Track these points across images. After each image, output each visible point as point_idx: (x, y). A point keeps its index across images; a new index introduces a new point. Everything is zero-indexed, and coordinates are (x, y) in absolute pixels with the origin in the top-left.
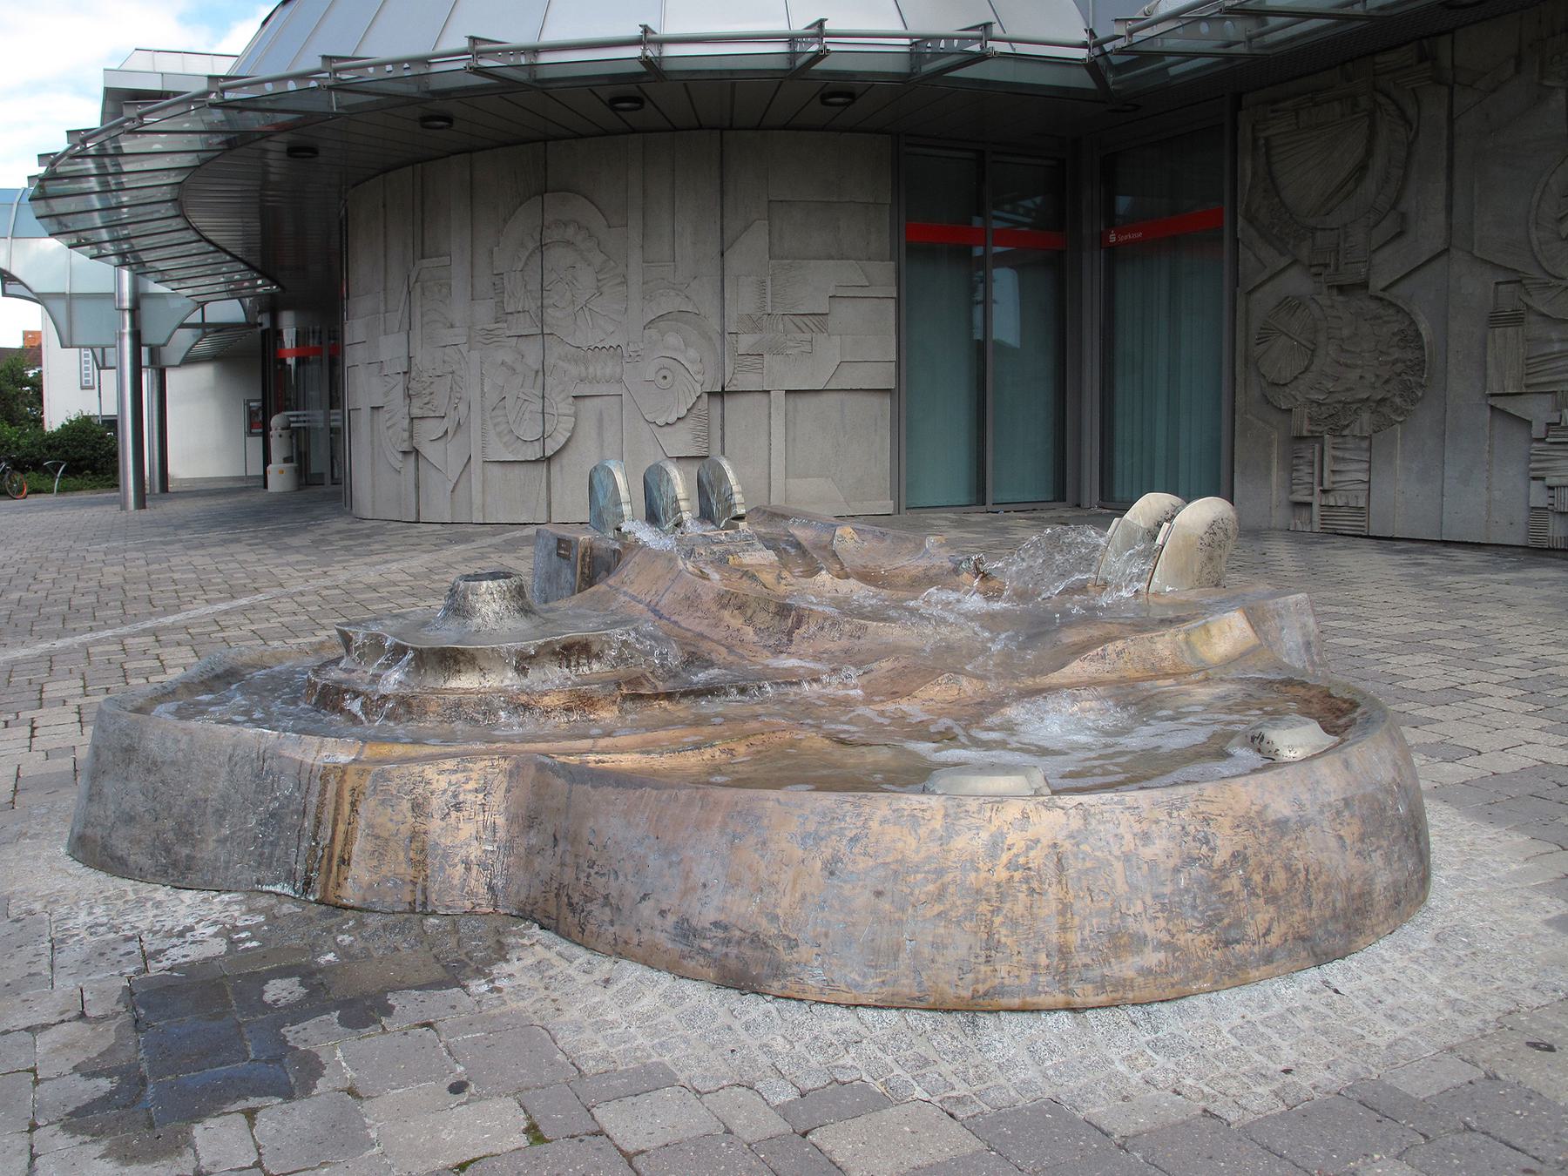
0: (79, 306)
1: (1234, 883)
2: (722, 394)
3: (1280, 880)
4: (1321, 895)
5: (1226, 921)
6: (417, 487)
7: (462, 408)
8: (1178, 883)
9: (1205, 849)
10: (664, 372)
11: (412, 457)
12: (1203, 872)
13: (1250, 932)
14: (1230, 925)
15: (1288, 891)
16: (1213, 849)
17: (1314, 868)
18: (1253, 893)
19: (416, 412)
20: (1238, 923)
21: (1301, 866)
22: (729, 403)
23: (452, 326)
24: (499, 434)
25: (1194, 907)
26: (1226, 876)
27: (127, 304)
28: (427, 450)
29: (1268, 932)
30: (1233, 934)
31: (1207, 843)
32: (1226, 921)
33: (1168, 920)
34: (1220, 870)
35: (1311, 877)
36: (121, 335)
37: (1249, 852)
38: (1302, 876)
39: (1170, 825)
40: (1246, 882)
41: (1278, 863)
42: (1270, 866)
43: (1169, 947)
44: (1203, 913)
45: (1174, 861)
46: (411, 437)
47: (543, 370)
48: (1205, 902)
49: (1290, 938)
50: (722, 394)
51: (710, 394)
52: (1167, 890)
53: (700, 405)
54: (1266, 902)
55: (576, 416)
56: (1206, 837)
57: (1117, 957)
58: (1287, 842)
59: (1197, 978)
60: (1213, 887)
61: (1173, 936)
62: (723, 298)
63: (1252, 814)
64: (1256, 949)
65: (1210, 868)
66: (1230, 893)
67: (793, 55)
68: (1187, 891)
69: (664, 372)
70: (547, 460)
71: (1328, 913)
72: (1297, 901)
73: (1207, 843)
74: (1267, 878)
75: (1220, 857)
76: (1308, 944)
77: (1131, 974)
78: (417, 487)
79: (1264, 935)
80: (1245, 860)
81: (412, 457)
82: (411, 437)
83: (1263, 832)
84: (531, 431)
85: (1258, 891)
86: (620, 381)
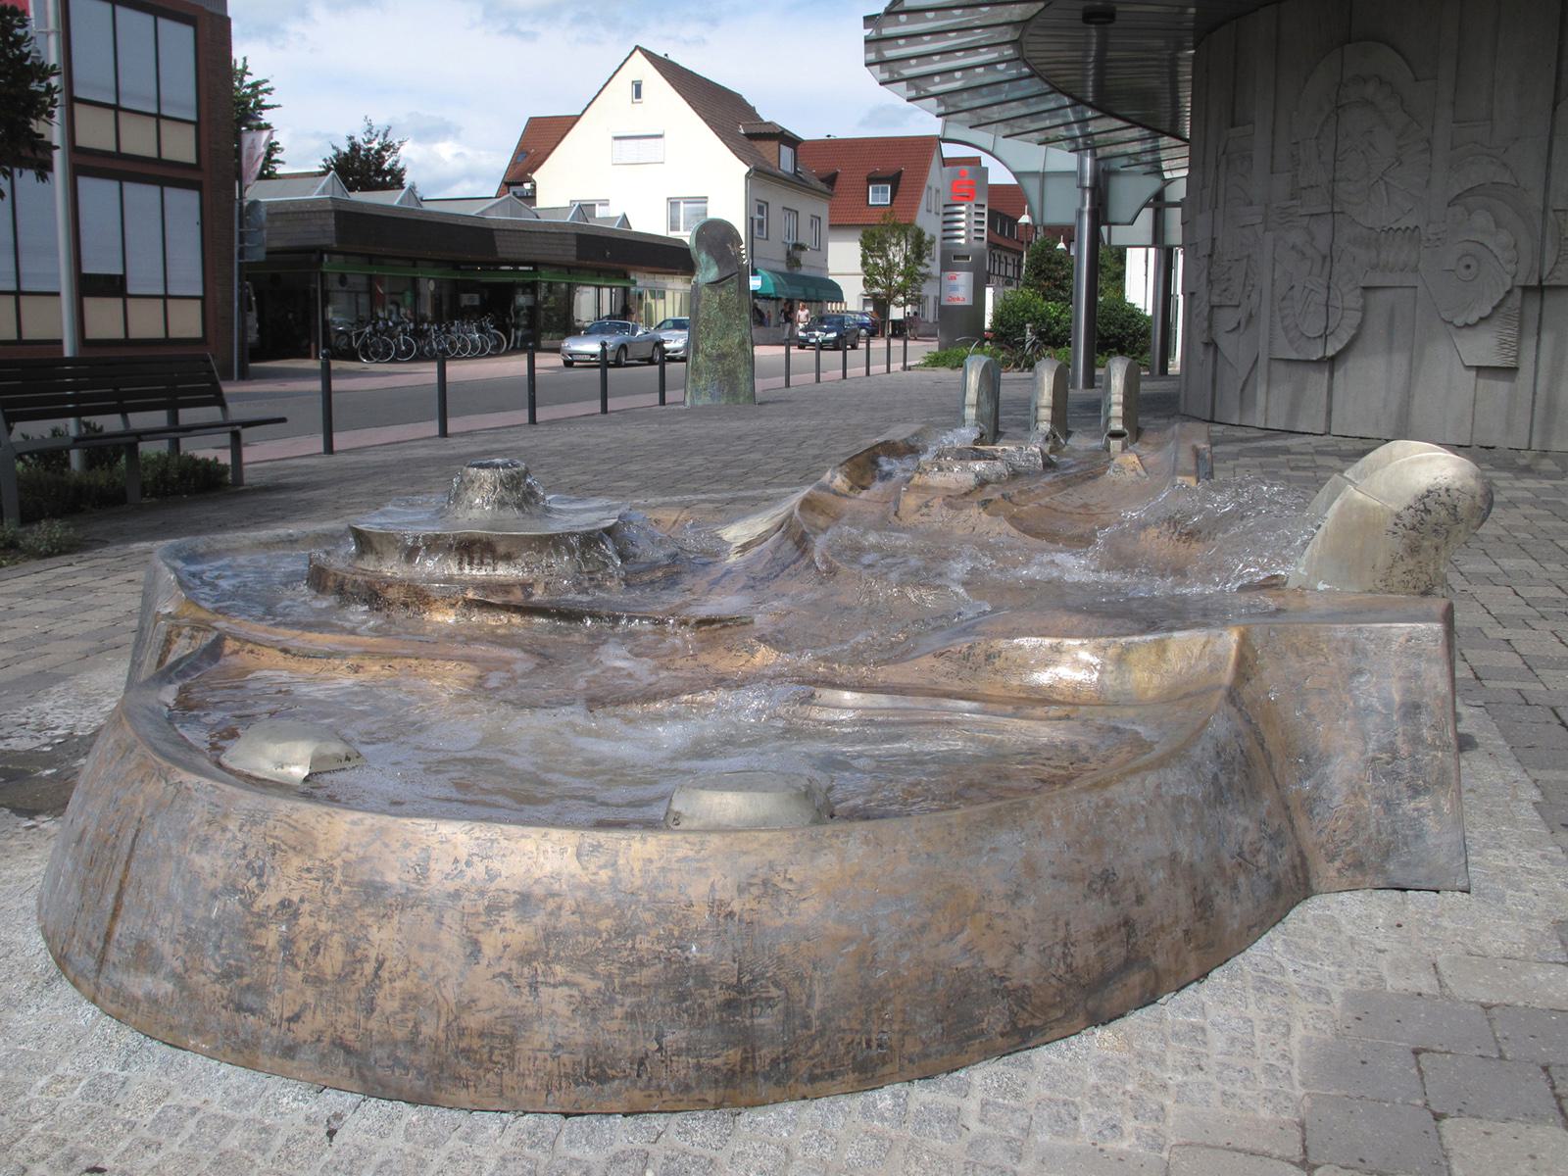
0: (1052, 185)
1: (271, 937)
2: (1541, 289)
3: (333, 960)
4: (395, 1005)
5: (246, 980)
6: (1214, 381)
7: (1255, 297)
8: (210, 911)
9: (253, 882)
10: (1468, 260)
11: (1211, 349)
12: (240, 908)
13: (271, 1006)
14: (249, 987)
15: (342, 978)
16: (262, 886)
17: (395, 964)
18: (290, 961)
19: (1215, 300)
20: (260, 989)
21: (373, 954)
22: (1551, 301)
23: (1251, 203)
24: (1285, 329)
25: (218, 947)
26: (262, 925)
27: (1088, 183)
28: (1225, 342)
29: (295, 1018)
30: (250, 999)
31: (260, 876)
32: (246, 980)
33: (188, 951)
34: (259, 915)
35: (384, 974)
36: (1080, 213)
37: (306, 907)
38: (369, 968)
39: (235, 838)
40: (287, 943)
41: (337, 937)
42: (326, 935)
43: (178, 979)
44: (224, 957)
45: (217, 883)
46: (1210, 327)
47: (1328, 258)
48: (231, 945)
49: (326, 1039)
50: (1541, 289)
51: (1525, 289)
52: (200, 913)
53: (1510, 302)
54: (305, 980)
55: (1364, 309)
56: (262, 868)
57: (137, 969)
58: (364, 915)
59: (197, 1031)
60: (245, 933)
61: (187, 971)
62: (1549, 165)
63: (337, 862)
64: (274, 1032)
65: (247, 906)
66: (262, 948)
67: (42, 72)
68: (217, 924)
69: (1468, 260)
70: (1331, 362)
71: (400, 1034)
72: (352, 996)
73: (260, 876)
74: (316, 949)
75: (270, 899)
76: (354, 1061)
77: (139, 993)
78: (1214, 381)
79: (290, 1020)
80: (296, 915)
81: (1211, 349)
82: (1210, 327)
83: (338, 890)
84: (1314, 327)
85: (299, 961)
86: (1415, 270)
